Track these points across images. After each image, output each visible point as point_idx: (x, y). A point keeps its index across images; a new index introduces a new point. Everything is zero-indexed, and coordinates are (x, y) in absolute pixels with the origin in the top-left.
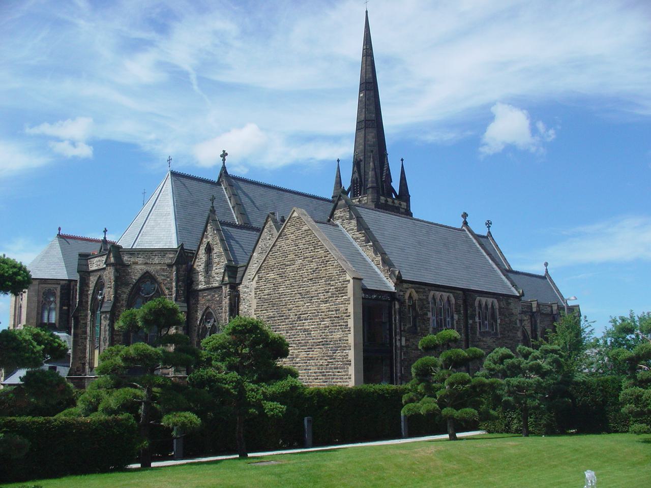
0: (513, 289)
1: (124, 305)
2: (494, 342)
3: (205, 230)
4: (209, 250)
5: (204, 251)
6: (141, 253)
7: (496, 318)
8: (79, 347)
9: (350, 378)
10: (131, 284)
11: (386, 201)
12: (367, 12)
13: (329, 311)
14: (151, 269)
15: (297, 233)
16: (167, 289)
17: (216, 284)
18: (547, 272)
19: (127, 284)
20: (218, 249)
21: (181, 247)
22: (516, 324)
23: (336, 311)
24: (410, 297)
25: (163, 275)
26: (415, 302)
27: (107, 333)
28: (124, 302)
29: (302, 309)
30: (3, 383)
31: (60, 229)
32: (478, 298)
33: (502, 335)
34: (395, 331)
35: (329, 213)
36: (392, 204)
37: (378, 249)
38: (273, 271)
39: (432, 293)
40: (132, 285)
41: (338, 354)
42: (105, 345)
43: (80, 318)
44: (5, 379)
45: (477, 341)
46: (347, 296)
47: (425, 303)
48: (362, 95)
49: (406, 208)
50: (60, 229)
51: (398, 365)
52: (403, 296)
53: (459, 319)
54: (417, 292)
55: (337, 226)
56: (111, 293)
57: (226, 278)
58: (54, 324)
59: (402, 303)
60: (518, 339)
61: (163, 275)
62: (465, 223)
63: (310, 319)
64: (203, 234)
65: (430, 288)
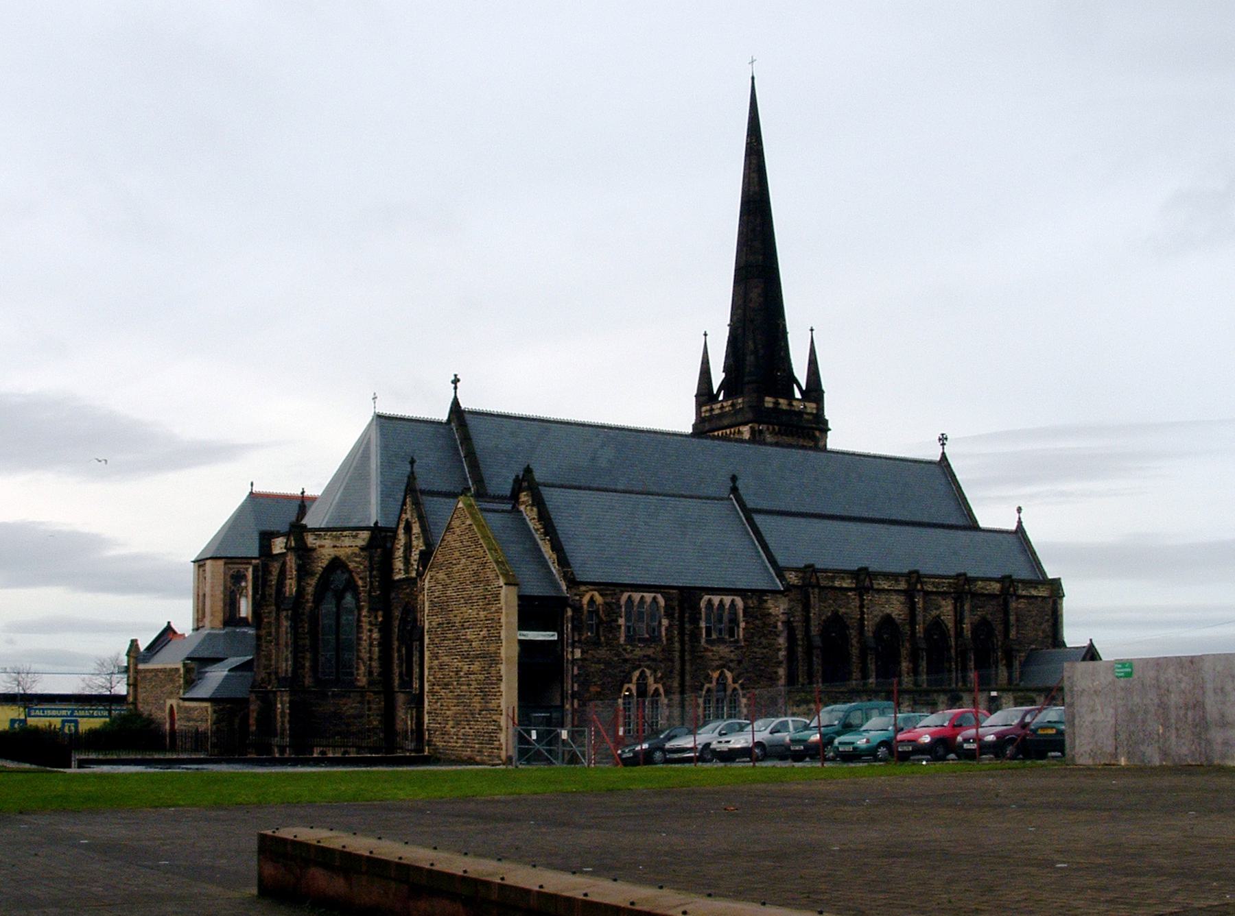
2: (732, 652)
3: (404, 503)
4: (408, 529)
5: (403, 531)
7: (739, 621)
8: (263, 653)
10: (316, 573)
11: (777, 403)
12: (753, 78)
13: (486, 620)
14: (341, 553)
16: (360, 578)
18: (1020, 522)
22: (776, 627)
24: (592, 600)
26: (598, 609)
27: (289, 635)
30: (183, 697)
31: (252, 484)
32: (706, 597)
33: (747, 643)
34: (567, 642)
36: (787, 408)
37: (557, 547)
39: (625, 596)
40: (318, 576)
43: (263, 615)
44: (184, 694)
45: (702, 652)
46: (499, 603)
47: (614, 607)
49: (815, 411)
50: (252, 484)
51: (570, 682)
52: (580, 601)
53: (670, 625)
54: (601, 595)
58: (245, 619)
59: (577, 609)
60: (779, 647)
61: (356, 562)
62: (734, 490)
63: (472, 628)
64: (402, 509)
65: (622, 589)
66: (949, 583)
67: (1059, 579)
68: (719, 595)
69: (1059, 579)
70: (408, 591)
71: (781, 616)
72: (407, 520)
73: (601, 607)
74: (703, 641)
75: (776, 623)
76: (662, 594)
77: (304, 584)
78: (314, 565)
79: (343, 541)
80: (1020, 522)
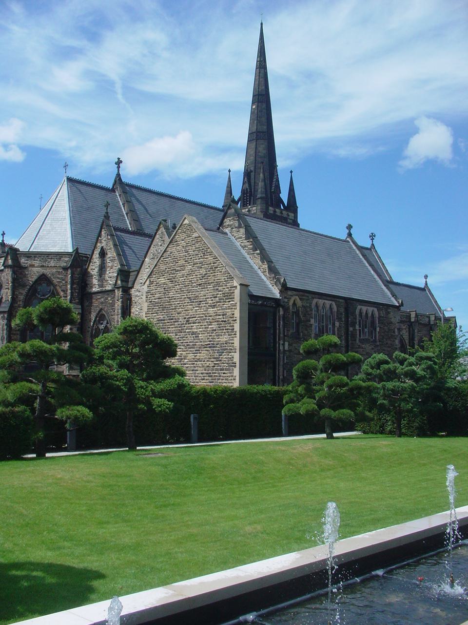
0: (393, 299)
1: (21, 306)
2: (373, 349)
3: (100, 235)
4: (103, 254)
5: (98, 256)
6: (38, 256)
7: (376, 326)
9: (235, 380)
10: (27, 285)
11: (275, 211)
12: (262, 24)
14: (47, 272)
15: (188, 240)
17: (109, 288)
18: (426, 284)
19: (24, 286)
20: (111, 254)
21: (76, 251)
22: (394, 332)
23: (223, 315)
24: (294, 304)
25: (58, 278)
27: (5, 332)
28: (21, 303)
29: (191, 312)
32: (359, 307)
33: (380, 343)
34: (279, 336)
35: (219, 222)
37: (264, 257)
38: (164, 276)
39: (315, 301)
40: (28, 287)
41: (224, 356)
42: (3, 344)
45: (357, 348)
48: (254, 107)
49: (293, 219)
52: (288, 302)
55: (226, 234)
56: (9, 294)
57: (119, 282)
59: (286, 309)
61: (58, 278)
62: (350, 235)
63: (199, 323)
64: (98, 239)
65: (313, 296)
66: (406, 315)
67: (455, 317)
68: (366, 306)
69: (455, 317)
70: (102, 299)
71: (397, 324)
72: (102, 247)
73: (300, 309)
74: (357, 340)
75: (394, 329)
76: (336, 302)
77: (17, 293)
78: (25, 279)
79: (49, 262)
80: (426, 284)
